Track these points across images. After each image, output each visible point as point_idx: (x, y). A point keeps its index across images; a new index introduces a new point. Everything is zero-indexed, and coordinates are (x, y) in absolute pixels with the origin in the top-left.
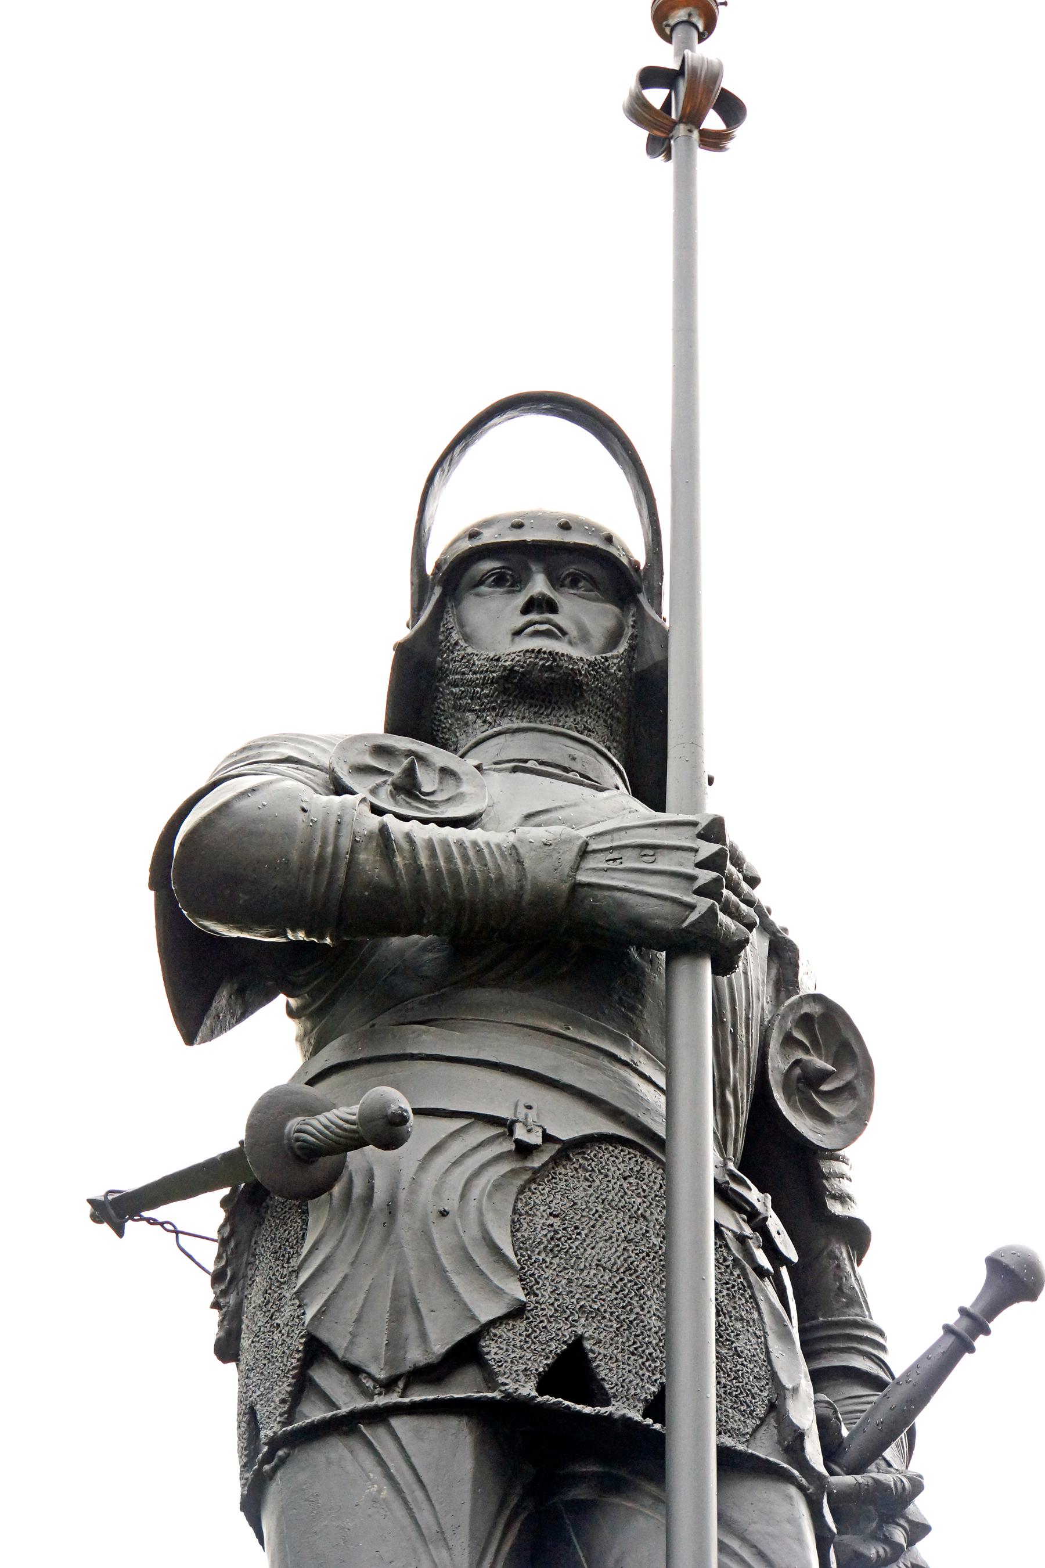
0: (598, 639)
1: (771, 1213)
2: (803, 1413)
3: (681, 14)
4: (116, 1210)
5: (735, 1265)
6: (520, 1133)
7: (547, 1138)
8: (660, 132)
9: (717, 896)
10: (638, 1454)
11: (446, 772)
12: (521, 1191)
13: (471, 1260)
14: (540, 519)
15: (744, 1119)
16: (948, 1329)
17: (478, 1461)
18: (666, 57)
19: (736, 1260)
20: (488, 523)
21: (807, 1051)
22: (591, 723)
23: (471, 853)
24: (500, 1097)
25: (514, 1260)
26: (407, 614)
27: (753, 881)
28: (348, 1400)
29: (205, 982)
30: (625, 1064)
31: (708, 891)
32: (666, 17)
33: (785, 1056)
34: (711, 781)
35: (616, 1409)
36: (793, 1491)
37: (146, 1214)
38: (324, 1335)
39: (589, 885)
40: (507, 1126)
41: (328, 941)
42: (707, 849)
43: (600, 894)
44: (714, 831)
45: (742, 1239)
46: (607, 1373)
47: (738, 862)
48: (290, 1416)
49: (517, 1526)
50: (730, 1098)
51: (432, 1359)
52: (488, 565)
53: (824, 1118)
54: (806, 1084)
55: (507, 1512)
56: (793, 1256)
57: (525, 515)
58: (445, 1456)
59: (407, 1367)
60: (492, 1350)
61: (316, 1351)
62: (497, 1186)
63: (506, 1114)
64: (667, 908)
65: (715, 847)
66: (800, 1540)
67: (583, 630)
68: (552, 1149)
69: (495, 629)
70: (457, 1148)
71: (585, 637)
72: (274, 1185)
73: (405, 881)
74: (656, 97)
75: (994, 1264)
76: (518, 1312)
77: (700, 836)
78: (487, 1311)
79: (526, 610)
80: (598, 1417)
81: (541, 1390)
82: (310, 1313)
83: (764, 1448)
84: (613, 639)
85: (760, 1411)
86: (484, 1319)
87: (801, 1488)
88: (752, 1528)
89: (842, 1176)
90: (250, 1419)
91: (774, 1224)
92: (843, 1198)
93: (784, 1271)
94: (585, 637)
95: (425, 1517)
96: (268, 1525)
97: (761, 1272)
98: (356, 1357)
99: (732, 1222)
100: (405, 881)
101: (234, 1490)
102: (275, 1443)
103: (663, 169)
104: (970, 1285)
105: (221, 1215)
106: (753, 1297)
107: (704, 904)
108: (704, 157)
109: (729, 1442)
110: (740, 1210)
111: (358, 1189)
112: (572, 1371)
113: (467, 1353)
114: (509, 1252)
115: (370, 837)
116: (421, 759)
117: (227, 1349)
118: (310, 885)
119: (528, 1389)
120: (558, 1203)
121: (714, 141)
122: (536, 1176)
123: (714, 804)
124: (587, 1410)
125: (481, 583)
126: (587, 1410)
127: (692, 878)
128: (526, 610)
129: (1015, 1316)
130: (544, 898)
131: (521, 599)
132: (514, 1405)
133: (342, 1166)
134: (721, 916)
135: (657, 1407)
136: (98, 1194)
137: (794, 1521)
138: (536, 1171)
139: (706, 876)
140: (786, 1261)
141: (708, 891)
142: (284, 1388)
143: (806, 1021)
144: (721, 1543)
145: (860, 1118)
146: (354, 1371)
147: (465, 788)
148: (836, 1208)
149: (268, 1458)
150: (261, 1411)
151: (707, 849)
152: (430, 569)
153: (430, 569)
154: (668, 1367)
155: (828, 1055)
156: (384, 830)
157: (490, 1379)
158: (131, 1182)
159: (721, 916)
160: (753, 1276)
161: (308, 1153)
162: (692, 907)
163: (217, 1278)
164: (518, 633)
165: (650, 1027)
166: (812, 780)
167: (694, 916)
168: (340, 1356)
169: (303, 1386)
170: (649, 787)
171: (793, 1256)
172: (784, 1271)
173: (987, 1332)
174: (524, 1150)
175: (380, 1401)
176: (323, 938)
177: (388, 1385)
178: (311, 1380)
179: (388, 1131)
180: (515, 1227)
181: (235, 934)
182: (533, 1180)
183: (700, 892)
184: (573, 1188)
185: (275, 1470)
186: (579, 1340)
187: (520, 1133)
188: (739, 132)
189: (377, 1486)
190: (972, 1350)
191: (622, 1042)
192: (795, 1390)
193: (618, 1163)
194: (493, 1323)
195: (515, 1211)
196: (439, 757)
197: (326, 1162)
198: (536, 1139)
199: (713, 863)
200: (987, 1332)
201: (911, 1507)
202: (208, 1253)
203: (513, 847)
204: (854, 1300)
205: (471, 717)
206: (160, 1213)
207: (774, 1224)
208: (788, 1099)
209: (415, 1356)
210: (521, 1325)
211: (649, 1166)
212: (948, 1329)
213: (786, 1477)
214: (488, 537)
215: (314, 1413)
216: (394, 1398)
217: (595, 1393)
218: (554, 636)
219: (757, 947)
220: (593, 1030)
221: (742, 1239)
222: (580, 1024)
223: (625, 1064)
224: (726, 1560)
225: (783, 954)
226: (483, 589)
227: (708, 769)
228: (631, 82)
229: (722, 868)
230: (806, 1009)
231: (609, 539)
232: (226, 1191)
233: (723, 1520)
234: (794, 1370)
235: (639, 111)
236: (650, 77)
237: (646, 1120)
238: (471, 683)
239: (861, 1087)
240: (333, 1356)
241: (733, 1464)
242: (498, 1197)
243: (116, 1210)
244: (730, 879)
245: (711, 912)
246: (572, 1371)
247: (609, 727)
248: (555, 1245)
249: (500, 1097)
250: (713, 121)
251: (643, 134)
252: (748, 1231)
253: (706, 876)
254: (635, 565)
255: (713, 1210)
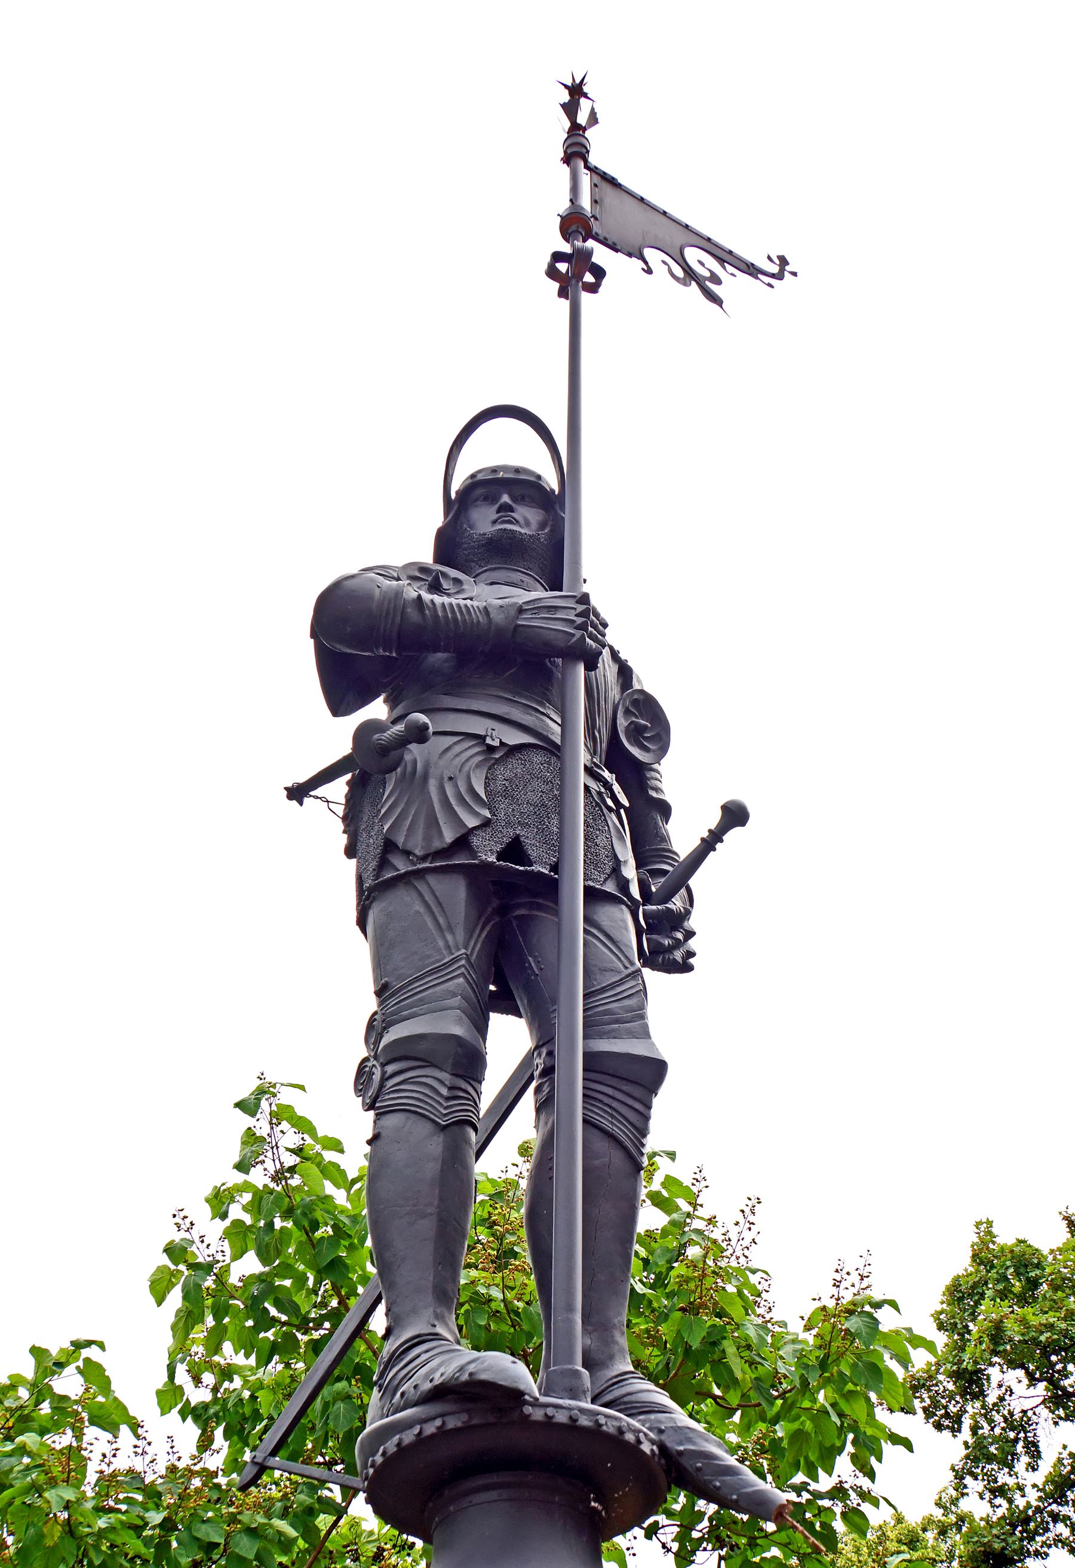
0: (534, 525)
1: (615, 782)
2: (630, 872)
3: (574, 228)
4: (298, 793)
5: (596, 806)
6: (489, 741)
7: (501, 743)
8: (568, 287)
9: (586, 630)
10: (548, 889)
11: (457, 581)
12: (490, 769)
13: (464, 799)
14: (505, 468)
15: (604, 745)
16: (703, 839)
17: (467, 896)
18: (566, 248)
19: (597, 803)
20: (480, 471)
21: (637, 717)
22: (531, 566)
23: (464, 610)
24: (478, 726)
25: (484, 796)
26: (442, 519)
27: (605, 625)
28: (402, 866)
29: (342, 687)
30: (543, 714)
31: (583, 627)
32: (567, 229)
33: (626, 719)
34: (585, 581)
35: (536, 868)
36: (624, 907)
37: (312, 793)
38: (393, 838)
39: (523, 626)
40: (481, 739)
41: (394, 655)
42: (581, 608)
43: (528, 630)
44: (584, 599)
45: (600, 793)
46: (533, 853)
47: (597, 615)
48: (377, 876)
49: (488, 929)
50: (597, 734)
51: (445, 846)
52: (479, 491)
53: (646, 749)
54: (636, 733)
55: (483, 919)
56: (627, 804)
57: (498, 467)
58: (455, 893)
59: (432, 850)
60: (476, 841)
61: (389, 846)
62: (478, 766)
63: (483, 733)
64: (560, 636)
65: (585, 607)
66: (627, 929)
67: (527, 521)
68: (506, 749)
69: (484, 521)
70: (457, 749)
71: (527, 524)
72: (369, 768)
73: (430, 621)
74: (562, 267)
75: (725, 808)
76: (486, 824)
77: (577, 602)
78: (471, 822)
79: (498, 512)
80: (526, 871)
81: (498, 860)
82: (386, 828)
83: (610, 887)
84: (542, 526)
85: (608, 871)
86: (470, 826)
87: (627, 906)
88: (603, 923)
89: (657, 779)
90: (360, 880)
91: (617, 788)
92: (657, 790)
93: (622, 811)
94: (527, 524)
95: (441, 920)
96: (370, 929)
97: (610, 809)
98: (409, 846)
99: (593, 785)
100: (430, 621)
101: (353, 914)
102: (371, 890)
103: (565, 304)
104: (714, 819)
105: (346, 789)
106: (605, 820)
107: (578, 634)
108: (585, 296)
109: (591, 884)
110: (600, 781)
111: (409, 769)
112: (514, 851)
113: (463, 843)
114: (484, 796)
115: (413, 600)
116: (444, 575)
117: (350, 851)
118: (383, 625)
119: (492, 859)
120: (508, 774)
121: (593, 288)
122: (497, 761)
123: (585, 588)
124: (522, 868)
125: (477, 500)
126: (522, 868)
127: (573, 621)
128: (498, 512)
129: (734, 835)
130: (500, 631)
131: (496, 506)
132: (486, 866)
133: (401, 758)
134: (588, 640)
135: (555, 868)
136: (290, 785)
137: (624, 921)
138: (497, 760)
139: (579, 620)
140: (623, 806)
141: (583, 627)
142: (374, 864)
143: (635, 703)
144: (585, 929)
145: (663, 750)
146: (407, 853)
147: (464, 587)
148: (654, 794)
149: (367, 898)
150: (365, 876)
151: (581, 608)
152: (453, 496)
153: (453, 496)
154: (560, 852)
155: (649, 721)
156: (419, 597)
157: (473, 854)
158: (302, 779)
159: (588, 640)
160: (605, 811)
161: (385, 750)
162: (573, 635)
163: (344, 819)
164: (494, 522)
165: (555, 691)
166: (635, 582)
167: (574, 639)
168: (400, 845)
169: (383, 863)
170: (555, 583)
171: (627, 804)
172: (622, 811)
173: (722, 841)
174: (491, 749)
175: (420, 866)
176: (391, 652)
177: (424, 859)
178: (388, 861)
179: (420, 734)
180: (487, 785)
181: (349, 651)
182: (494, 765)
183: (577, 628)
184: (514, 767)
185: (372, 902)
186: (517, 837)
187: (489, 741)
188: (605, 282)
189: (419, 907)
190: (715, 850)
191: (544, 706)
192: (626, 862)
193: (538, 758)
194: (475, 828)
195: (487, 778)
196: (453, 573)
197: (394, 754)
198: (496, 743)
199: (584, 614)
200: (722, 841)
201: (686, 923)
202: (340, 810)
203: (485, 608)
204: (664, 839)
205: (473, 564)
206: (319, 792)
207: (617, 788)
208: (631, 743)
209: (437, 845)
210: (489, 830)
211: (553, 759)
212: (703, 839)
213: (621, 902)
214: (480, 477)
215: (389, 875)
216: (427, 865)
217: (525, 860)
218: (511, 521)
219: (606, 652)
220: (526, 698)
221: (600, 793)
222: (521, 695)
223: (543, 714)
224: (590, 938)
225: (625, 672)
226: (479, 503)
227: (584, 577)
228: (548, 259)
229: (589, 620)
230: (636, 697)
231: (539, 477)
232: (348, 776)
233: (587, 920)
234: (626, 854)
235: (552, 273)
236: (557, 257)
237: (553, 738)
238: (473, 548)
239: (663, 735)
240: (397, 847)
241: (593, 895)
242: (478, 771)
243: (298, 793)
244: (592, 622)
245: (583, 637)
246: (514, 851)
247: (541, 568)
248: (506, 794)
249: (478, 726)
250: (589, 278)
251: (557, 285)
252: (603, 790)
253: (579, 620)
254: (553, 491)
255: (582, 778)
